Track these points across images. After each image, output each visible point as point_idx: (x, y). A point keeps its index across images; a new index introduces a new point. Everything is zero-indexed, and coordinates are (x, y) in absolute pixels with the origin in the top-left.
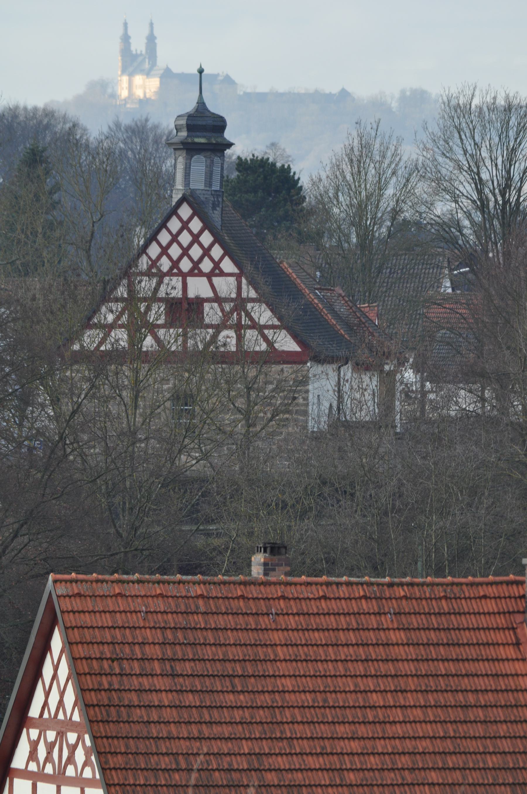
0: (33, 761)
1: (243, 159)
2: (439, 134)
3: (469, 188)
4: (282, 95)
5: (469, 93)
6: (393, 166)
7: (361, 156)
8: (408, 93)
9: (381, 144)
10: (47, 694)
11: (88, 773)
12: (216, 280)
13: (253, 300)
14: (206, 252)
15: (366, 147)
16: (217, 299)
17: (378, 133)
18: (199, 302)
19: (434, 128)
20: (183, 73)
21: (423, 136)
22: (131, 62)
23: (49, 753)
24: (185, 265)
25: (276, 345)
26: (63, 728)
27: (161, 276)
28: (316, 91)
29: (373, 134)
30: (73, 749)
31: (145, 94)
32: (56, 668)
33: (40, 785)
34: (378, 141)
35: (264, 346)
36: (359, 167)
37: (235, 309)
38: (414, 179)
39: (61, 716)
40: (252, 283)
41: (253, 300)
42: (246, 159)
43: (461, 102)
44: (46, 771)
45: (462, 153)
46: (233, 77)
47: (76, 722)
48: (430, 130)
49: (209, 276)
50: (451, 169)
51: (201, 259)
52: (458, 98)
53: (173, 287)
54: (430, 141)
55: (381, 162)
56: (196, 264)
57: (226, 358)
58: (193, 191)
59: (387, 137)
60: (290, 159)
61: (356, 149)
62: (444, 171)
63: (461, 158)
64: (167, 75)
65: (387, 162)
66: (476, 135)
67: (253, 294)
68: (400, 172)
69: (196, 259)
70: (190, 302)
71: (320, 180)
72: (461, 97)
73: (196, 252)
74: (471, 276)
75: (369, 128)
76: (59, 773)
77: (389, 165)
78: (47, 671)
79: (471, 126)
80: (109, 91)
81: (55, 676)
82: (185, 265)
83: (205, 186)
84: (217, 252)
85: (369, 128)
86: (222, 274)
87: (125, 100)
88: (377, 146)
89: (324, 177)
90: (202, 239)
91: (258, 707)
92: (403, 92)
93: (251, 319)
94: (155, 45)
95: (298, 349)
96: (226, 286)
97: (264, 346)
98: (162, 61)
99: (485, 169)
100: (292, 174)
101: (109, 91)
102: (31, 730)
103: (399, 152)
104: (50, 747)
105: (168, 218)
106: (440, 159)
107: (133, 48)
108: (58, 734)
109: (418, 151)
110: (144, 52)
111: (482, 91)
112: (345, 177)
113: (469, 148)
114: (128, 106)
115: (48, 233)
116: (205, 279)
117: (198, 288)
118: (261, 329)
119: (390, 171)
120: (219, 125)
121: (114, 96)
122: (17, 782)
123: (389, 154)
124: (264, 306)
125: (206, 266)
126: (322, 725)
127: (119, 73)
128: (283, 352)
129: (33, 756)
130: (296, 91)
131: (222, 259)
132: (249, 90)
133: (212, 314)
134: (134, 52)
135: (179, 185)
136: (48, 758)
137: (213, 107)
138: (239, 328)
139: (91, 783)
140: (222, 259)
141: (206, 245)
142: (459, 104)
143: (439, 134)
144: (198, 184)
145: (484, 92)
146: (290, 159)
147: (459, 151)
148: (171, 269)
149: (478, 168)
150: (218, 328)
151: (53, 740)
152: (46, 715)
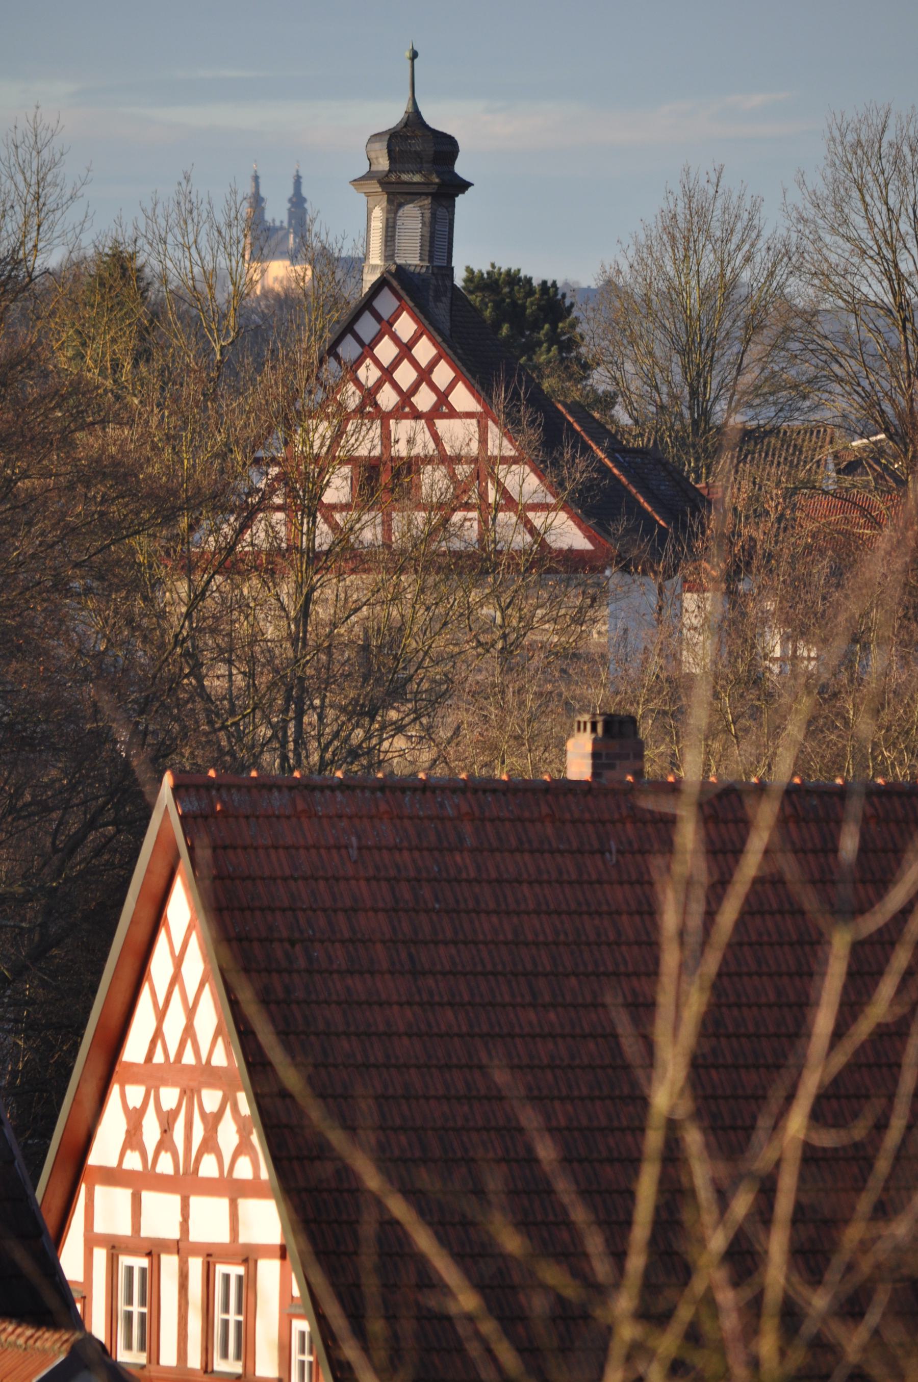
0: (133, 1149)
1: (476, 271)
2: (826, 192)
5: (878, 121)
6: (746, 247)
7: (690, 230)
9: (725, 210)
10: (161, 1015)
11: (244, 1170)
12: (442, 425)
13: (504, 460)
14: (425, 375)
15: (699, 214)
17: (720, 191)
18: (412, 466)
19: (818, 184)
21: (797, 197)
24: (387, 398)
25: (549, 539)
29: (712, 192)
30: (212, 1122)
33: (147, 1196)
34: (719, 203)
36: (687, 249)
38: (781, 272)
39: (189, 1058)
42: (480, 272)
43: (863, 138)
44: (159, 1170)
45: (866, 226)
47: (217, 1068)
48: (810, 189)
50: (847, 255)
51: (415, 388)
52: (857, 130)
53: (366, 443)
54: (809, 206)
55: (726, 241)
56: (406, 397)
58: (399, 268)
59: (734, 198)
61: (680, 218)
62: (833, 258)
63: (864, 234)
65: (735, 239)
66: (891, 194)
68: (758, 259)
71: (619, 272)
72: (864, 127)
73: (405, 375)
75: (703, 182)
76: (185, 1173)
77: (739, 248)
78: (160, 965)
79: (881, 180)
81: (176, 978)
82: (387, 398)
84: (443, 374)
85: (703, 182)
86: (453, 414)
88: (718, 213)
89: (625, 268)
90: (413, 375)
91: (584, 1037)
99: (907, 255)
100: (559, 297)
102: (129, 1089)
103: (756, 222)
104: (167, 1121)
105: (356, 316)
106: (828, 238)
107: (268, 216)
108: (183, 1092)
109: (788, 223)
110: (286, 224)
111: (900, 117)
112: (661, 267)
113: (878, 220)
117: (409, 438)
119: (740, 256)
120: (445, 148)
123: (739, 226)
125: (424, 400)
126: (713, 1072)
129: (133, 1139)
131: (452, 386)
133: (433, 481)
135: (376, 258)
137: (437, 117)
140: (452, 386)
141: (424, 363)
142: (859, 141)
143: (826, 192)
145: (904, 119)
147: (859, 221)
149: (894, 252)
151: (174, 1106)
152: (159, 1058)
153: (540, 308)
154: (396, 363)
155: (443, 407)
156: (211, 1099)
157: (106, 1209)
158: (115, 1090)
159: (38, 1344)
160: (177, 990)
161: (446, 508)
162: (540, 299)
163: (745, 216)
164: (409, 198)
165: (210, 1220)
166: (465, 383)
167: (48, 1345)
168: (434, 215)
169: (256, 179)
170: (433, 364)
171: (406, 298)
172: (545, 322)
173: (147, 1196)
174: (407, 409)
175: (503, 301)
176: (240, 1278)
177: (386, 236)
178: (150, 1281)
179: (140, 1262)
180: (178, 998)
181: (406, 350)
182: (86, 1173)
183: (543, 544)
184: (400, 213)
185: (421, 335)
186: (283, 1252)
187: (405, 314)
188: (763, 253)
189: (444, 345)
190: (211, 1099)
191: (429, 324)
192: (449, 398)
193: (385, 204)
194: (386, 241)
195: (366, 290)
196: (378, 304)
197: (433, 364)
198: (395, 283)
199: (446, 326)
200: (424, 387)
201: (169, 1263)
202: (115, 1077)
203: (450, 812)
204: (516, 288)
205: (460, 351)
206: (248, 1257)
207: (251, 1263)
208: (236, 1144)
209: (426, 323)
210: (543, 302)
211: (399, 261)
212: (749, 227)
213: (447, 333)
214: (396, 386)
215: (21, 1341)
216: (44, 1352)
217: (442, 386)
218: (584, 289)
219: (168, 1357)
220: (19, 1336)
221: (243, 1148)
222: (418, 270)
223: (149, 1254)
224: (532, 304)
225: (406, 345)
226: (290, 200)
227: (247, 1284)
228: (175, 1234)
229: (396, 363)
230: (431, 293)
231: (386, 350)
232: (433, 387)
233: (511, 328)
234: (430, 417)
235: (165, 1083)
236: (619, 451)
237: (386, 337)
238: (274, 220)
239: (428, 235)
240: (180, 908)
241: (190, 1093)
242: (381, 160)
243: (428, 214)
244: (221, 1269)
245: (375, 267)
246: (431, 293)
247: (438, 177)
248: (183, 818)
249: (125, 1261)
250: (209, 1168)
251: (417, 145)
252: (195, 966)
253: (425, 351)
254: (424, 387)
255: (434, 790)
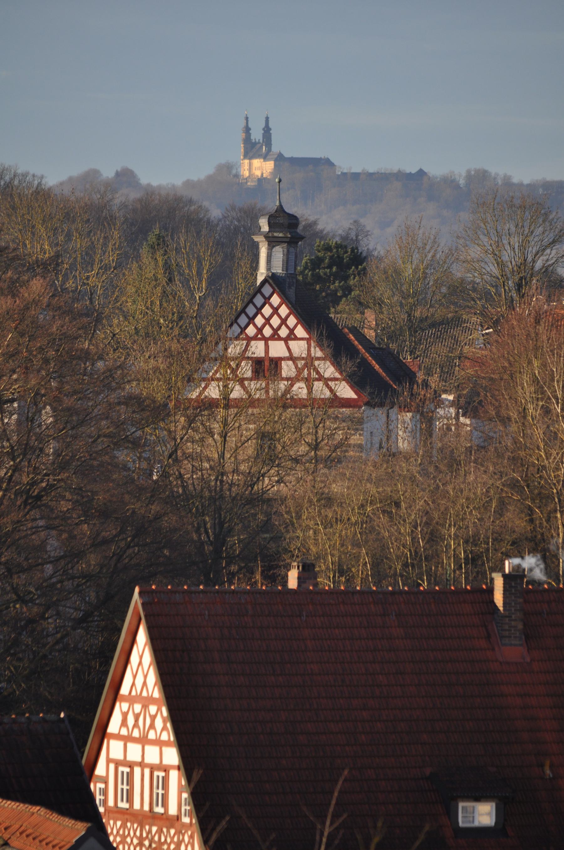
3: (493, 268)
4: (371, 175)
8: (473, 173)
10: (135, 677)
11: (165, 737)
12: (291, 343)
13: (318, 359)
14: (284, 321)
16: (291, 358)
17: (421, 226)
20: (292, 157)
22: (251, 149)
23: (137, 720)
24: (267, 332)
26: (146, 702)
27: (249, 339)
28: (399, 171)
29: (417, 226)
30: (153, 718)
31: (262, 174)
32: (141, 657)
33: (129, 745)
35: (328, 394)
37: (306, 365)
39: (145, 694)
40: (320, 345)
41: (318, 359)
46: (332, 160)
49: (286, 340)
50: (479, 253)
51: (279, 327)
53: (258, 349)
55: (424, 248)
56: (276, 331)
57: (298, 403)
58: (273, 274)
60: (369, 233)
64: (280, 159)
65: (428, 247)
67: (319, 354)
69: (275, 326)
70: (272, 360)
73: (275, 321)
74: (495, 337)
78: (134, 658)
80: (234, 172)
81: (140, 663)
82: (267, 332)
83: (283, 270)
84: (292, 321)
86: (296, 338)
87: (246, 179)
88: (421, 235)
92: (469, 171)
93: (318, 373)
94: (270, 135)
95: (354, 396)
96: (298, 348)
97: (328, 394)
98: (276, 148)
101: (234, 172)
108: (143, 707)
110: (261, 141)
114: (249, 184)
115: (165, 305)
116: (283, 342)
117: (277, 349)
118: (326, 381)
121: (237, 176)
122: (113, 743)
124: (328, 363)
125: (284, 332)
127: (242, 157)
128: (343, 399)
129: (124, 723)
130: (383, 171)
131: (295, 326)
132: (345, 171)
133: (288, 369)
134: (254, 141)
136: (136, 725)
138: (309, 382)
139: (167, 744)
140: (295, 326)
141: (283, 316)
144: (278, 269)
146: (369, 233)
148: (256, 335)
150: (292, 381)
152: (133, 693)
153: (350, 259)
154: (271, 316)
155: (292, 336)
156: (153, 709)
157: (114, 749)
158: (118, 704)
159: (76, 827)
160: (140, 668)
161: (292, 381)
162: (351, 255)
163: (432, 237)
164: (277, 243)
165: (152, 755)
166: (301, 325)
167: (79, 827)
168: (288, 251)
169: (247, 119)
170: (287, 317)
171: (276, 288)
172: (352, 266)
173: (129, 745)
174: (276, 337)
175: (334, 255)
176: (163, 777)
177: (267, 260)
178: (130, 776)
179: (127, 770)
180: (141, 672)
181: (275, 311)
182: (107, 735)
183: (335, 395)
184: (274, 250)
185: (282, 304)
186: (179, 768)
187: (275, 294)
188: (441, 253)
189: (292, 309)
190: (153, 709)
191: (285, 299)
192: (295, 332)
193: (267, 246)
194: (267, 262)
195: (258, 284)
196: (264, 290)
197: (287, 317)
198: (271, 281)
199: (293, 299)
200: (283, 326)
201: (137, 771)
202: (118, 699)
203: (243, 601)
204: (340, 249)
205: (299, 310)
206: (166, 769)
207: (167, 772)
208: (162, 728)
209: (285, 299)
210: (352, 256)
211: (273, 271)
212: (434, 242)
213: (294, 302)
214: (271, 326)
215: (70, 825)
216: (77, 830)
217: (291, 326)
218: (408, 174)
219: (137, 806)
220: (70, 823)
221: (164, 728)
222: (281, 275)
223: (130, 767)
224: (347, 257)
225: (276, 308)
226: (263, 129)
227: (166, 780)
228: (139, 759)
229: (271, 316)
230: (287, 285)
231: (267, 311)
232: (287, 327)
233: (337, 268)
234: (286, 340)
235: (136, 702)
236: (372, 349)
237: (267, 305)
238: (255, 139)
239: (285, 259)
240: (142, 637)
241: (145, 707)
242: (265, 227)
243: (285, 250)
244: (156, 773)
245: (262, 274)
246: (287, 285)
247: (290, 234)
248: (143, 604)
249: (121, 769)
250: (152, 735)
251: (281, 220)
252: (148, 658)
253: (284, 311)
254: (283, 326)
255: (237, 593)
